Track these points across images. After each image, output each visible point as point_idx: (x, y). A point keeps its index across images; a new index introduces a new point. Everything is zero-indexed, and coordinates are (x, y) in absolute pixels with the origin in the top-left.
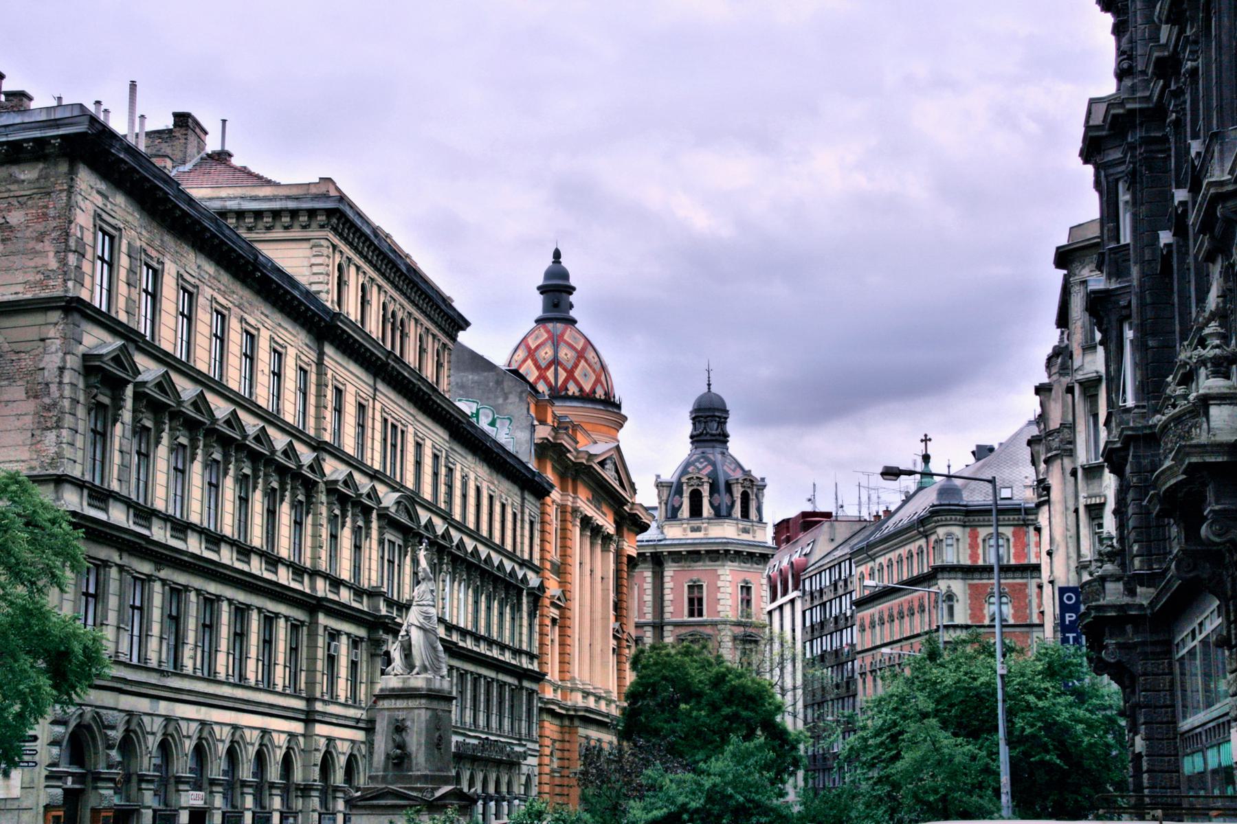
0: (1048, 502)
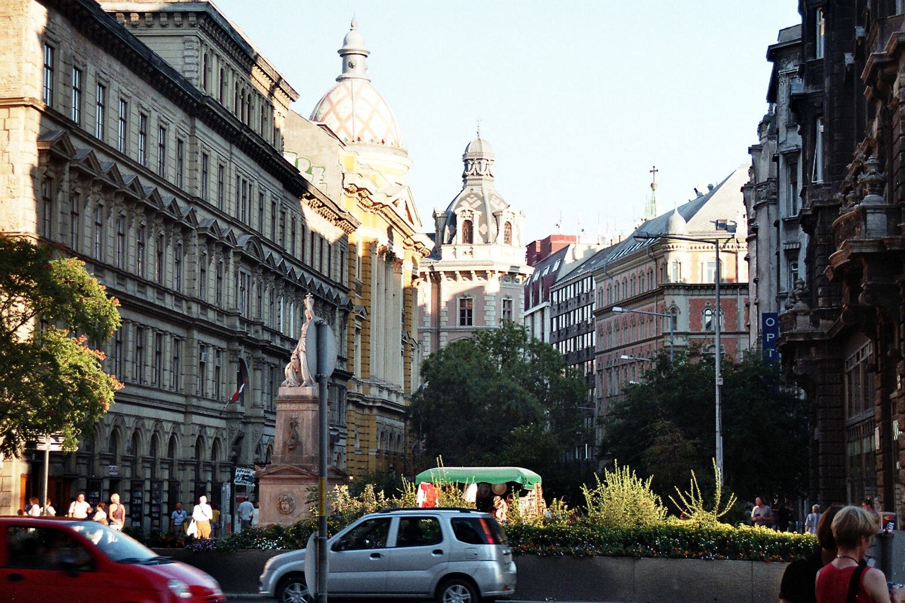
0: (756, 237)
